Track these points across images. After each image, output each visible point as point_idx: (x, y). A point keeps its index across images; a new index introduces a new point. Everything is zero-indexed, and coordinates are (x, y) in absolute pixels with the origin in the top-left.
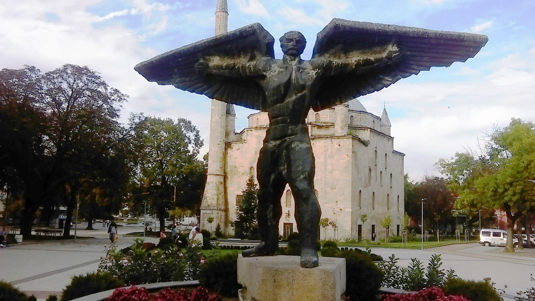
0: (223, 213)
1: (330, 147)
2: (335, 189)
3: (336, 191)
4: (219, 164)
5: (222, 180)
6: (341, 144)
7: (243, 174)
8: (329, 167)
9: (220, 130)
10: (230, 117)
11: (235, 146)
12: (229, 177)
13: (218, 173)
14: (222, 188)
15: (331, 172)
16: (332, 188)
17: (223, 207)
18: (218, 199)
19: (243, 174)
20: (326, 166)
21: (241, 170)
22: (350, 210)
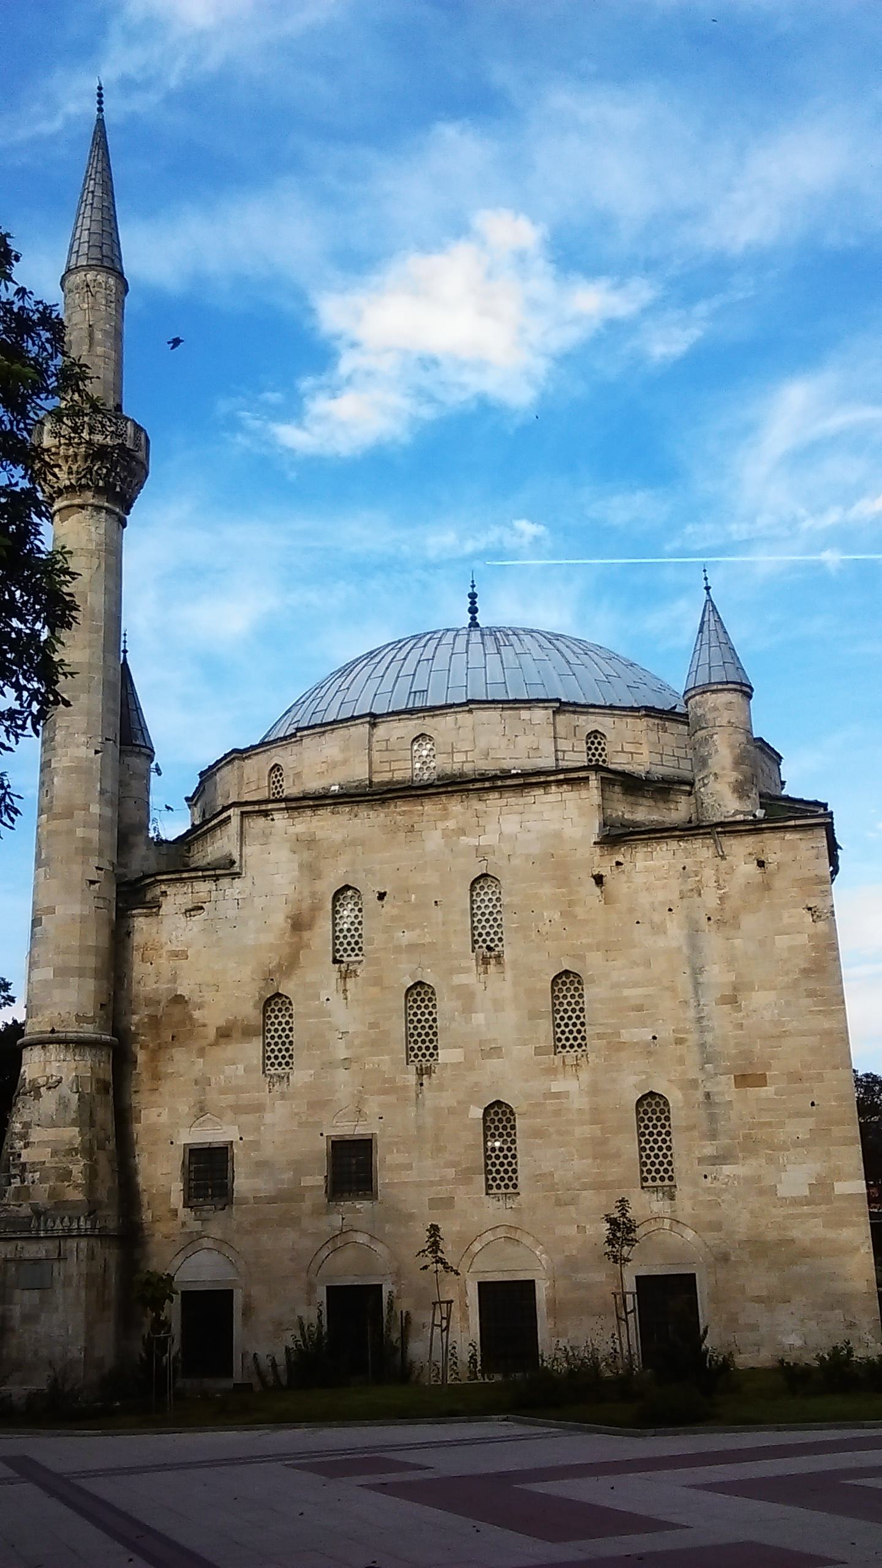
0: (110, 1255)
1: (708, 874)
2: (760, 1080)
3: (767, 1091)
4: (90, 984)
5: (106, 1072)
6: (771, 858)
7: (224, 1034)
8: (717, 975)
9: (95, 809)
10: (137, 762)
11: (175, 898)
12: (141, 1056)
13: (89, 1031)
14: (105, 1115)
15: (732, 1000)
16: (744, 1080)
17: (111, 1220)
18: (92, 1173)
19: (224, 1034)
20: (697, 972)
21: (211, 1015)
22: (859, 1186)
